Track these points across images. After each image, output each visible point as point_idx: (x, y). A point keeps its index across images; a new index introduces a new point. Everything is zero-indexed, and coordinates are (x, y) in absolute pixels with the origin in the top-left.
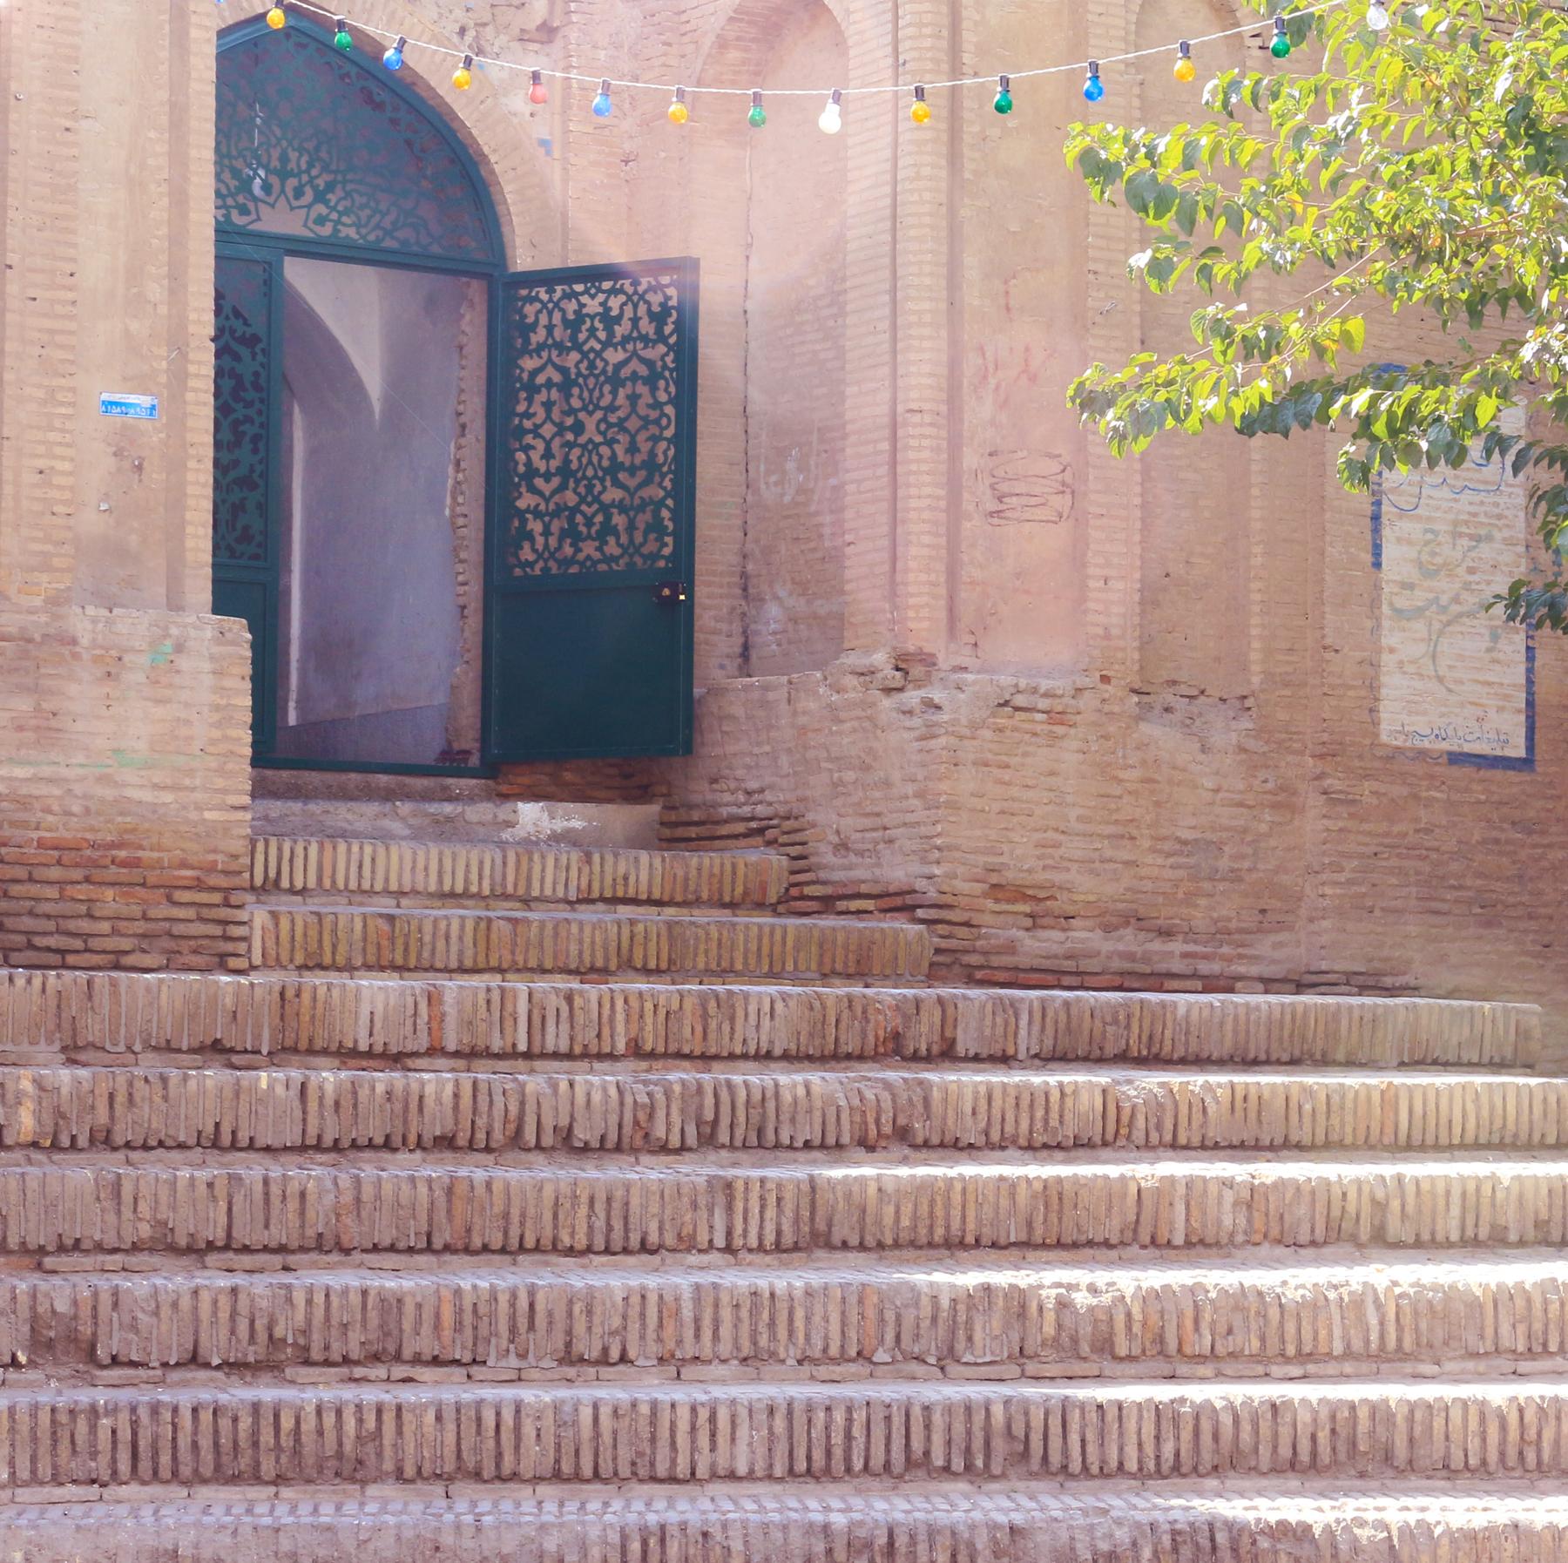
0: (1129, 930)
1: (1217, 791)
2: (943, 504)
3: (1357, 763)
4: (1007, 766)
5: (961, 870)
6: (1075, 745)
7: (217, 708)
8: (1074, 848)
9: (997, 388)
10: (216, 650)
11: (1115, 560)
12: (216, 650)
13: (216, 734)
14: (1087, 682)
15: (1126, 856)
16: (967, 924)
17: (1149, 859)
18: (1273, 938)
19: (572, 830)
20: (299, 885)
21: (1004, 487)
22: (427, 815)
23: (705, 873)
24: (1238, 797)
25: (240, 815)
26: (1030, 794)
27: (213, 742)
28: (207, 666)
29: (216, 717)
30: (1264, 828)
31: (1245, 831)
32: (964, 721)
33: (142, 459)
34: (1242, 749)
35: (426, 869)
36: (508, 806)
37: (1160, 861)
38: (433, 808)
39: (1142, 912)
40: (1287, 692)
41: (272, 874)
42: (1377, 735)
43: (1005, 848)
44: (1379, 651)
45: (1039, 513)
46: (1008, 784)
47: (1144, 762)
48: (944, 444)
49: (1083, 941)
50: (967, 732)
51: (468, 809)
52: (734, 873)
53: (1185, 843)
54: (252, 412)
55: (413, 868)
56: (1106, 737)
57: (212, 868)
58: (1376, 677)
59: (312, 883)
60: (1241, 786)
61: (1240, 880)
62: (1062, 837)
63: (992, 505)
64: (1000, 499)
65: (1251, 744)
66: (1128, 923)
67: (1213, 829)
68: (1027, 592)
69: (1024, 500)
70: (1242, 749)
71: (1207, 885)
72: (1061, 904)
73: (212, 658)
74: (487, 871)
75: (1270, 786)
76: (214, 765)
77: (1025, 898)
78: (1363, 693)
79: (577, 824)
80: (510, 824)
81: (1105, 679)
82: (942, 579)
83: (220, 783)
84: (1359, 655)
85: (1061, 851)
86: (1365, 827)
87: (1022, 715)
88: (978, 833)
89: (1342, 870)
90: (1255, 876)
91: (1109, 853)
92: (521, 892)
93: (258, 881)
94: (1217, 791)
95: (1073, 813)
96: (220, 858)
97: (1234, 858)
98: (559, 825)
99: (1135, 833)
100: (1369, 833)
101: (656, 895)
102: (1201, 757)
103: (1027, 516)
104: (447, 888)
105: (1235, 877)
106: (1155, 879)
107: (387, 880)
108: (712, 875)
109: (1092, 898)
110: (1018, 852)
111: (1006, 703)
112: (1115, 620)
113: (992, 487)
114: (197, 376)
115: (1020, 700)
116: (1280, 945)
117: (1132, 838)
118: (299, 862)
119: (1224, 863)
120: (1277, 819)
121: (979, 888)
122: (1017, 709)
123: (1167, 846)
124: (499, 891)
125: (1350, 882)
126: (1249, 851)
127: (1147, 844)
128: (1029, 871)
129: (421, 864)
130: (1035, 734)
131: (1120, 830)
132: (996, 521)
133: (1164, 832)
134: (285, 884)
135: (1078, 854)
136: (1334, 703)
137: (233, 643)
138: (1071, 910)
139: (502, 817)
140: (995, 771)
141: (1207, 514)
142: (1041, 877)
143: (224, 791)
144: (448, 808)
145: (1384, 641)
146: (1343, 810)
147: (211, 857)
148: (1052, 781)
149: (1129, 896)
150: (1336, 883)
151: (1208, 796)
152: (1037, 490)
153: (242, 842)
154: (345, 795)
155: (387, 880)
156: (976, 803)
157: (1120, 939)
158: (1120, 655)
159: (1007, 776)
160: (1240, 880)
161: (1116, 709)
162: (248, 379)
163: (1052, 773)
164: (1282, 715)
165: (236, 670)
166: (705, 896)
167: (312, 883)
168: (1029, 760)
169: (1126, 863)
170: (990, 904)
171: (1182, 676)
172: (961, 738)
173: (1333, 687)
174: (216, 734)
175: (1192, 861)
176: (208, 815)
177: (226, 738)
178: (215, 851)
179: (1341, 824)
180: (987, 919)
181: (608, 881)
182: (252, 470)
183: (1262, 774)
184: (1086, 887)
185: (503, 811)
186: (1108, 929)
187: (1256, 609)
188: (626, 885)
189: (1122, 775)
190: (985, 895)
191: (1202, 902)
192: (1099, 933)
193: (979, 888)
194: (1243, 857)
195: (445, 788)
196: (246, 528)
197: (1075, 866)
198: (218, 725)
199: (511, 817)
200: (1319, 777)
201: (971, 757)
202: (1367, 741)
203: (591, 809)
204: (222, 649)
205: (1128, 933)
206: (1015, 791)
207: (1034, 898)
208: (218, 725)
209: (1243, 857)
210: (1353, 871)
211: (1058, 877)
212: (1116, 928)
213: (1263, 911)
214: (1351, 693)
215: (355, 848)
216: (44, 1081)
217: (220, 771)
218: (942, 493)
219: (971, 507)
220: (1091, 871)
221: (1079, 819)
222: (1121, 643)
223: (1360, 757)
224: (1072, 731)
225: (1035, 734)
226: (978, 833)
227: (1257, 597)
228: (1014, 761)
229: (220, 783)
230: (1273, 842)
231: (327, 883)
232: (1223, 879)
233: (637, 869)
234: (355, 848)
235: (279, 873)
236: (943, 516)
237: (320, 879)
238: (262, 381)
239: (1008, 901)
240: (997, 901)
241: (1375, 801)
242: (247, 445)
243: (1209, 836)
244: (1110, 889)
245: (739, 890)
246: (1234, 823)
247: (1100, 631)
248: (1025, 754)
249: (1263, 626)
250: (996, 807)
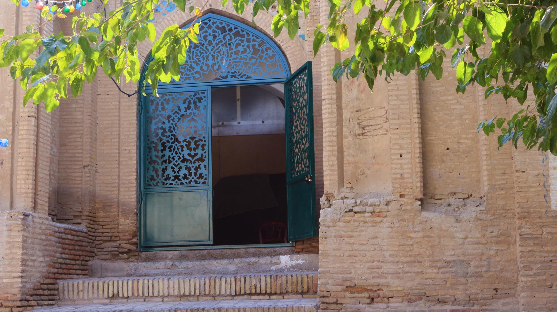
0: (422, 301)
1: (466, 238)
2: (335, 134)
3: (538, 220)
4: (352, 237)
5: (330, 281)
6: (387, 225)
7: (9, 243)
8: (388, 268)
9: (359, 85)
10: (8, 222)
11: (405, 146)
12: (8, 222)
13: (8, 252)
14: (392, 198)
15: (416, 270)
16: (336, 303)
17: (430, 271)
18: (502, 301)
19: (298, 264)
20: (126, 296)
21: (365, 123)
22: (246, 262)
23: (290, 282)
24: (477, 240)
25: (16, 280)
26: (364, 247)
27: (7, 255)
28: (5, 229)
29: (8, 246)
30: (492, 252)
31: (482, 254)
32: (329, 220)
33: (3, 160)
34: (478, 219)
35: (173, 287)
36: (277, 257)
37: (435, 271)
38: (247, 260)
39: (428, 293)
40: (503, 192)
41: (116, 292)
42: (550, 207)
43: (353, 271)
44: (548, 170)
45: (381, 132)
46: (353, 244)
47: (424, 230)
48: (335, 110)
49: (396, 307)
50: (331, 224)
51: (261, 260)
52: (302, 281)
53: (449, 262)
54: (169, 139)
55: (168, 287)
56: (403, 220)
57: (6, 299)
58: (547, 181)
59: (130, 295)
60: (478, 235)
61: (482, 276)
62: (382, 264)
63: (360, 131)
64: (363, 128)
65: (483, 217)
66: (421, 299)
67: (464, 255)
68: (378, 164)
69: (374, 127)
70: (478, 219)
71: (463, 280)
72: (386, 292)
73: (7, 225)
74: (197, 287)
75: (494, 234)
76: (7, 263)
77: (367, 290)
78: (539, 189)
79: (300, 262)
80: (278, 264)
81: (401, 196)
82: (335, 163)
83: (9, 269)
84: (536, 172)
85: (381, 270)
86: (545, 249)
87: (359, 215)
88: (338, 265)
89: (532, 269)
90: (489, 274)
91: (407, 269)
92: (212, 293)
93: (111, 295)
94: (466, 238)
95: (387, 254)
96: (9, 295)
97: (477, 267)
98: (294, 263)
99: (421, 259)
100: (547, 251)
101: (269, 291)
102: (456, 224)
103: (375, 133)
104: (182, 293)
105: (478, 275)
106: (433, 279)
107: (159, 292)
108: (292, 283)
109: (399, 289)
110: (359, 272)
111: (351, 211)
112: (406, 171)
113: (359, 124)
114: (22, 130)
115: (356, 209)
116: (508, 304)
117: (419, 262)
118: (125, 287)
119: (471, 270)
120: (500, 248)
121: (339, 288)
122: (356, 213)
123: (439, 264)
124: (203, 293)
125: (535, 274)
126: (485, 263)
127: (427, 264)
128: (366, 279)
129: (171, 286)
130: (365, 222)
131: (413, 259)
132: (362, 137)
133: (437, 258)
134: (121, 295)
135: (391, 271)
136: (523, 195)
137: (15, 220)
138: (390, 295)
139: (274, 261)
140: (347, 240)
141: (467, 121)
142: (372, 281)
143: (11, 272)
144: (253, 260)
145: (550, 165)
146: (531, 242)
147: (6, 295)
148: (375, 241)
149: (419, 287)
150: (528, 276)
151: (461, 241)
152: (378, 123)
153: (18, 289)
154: (216, 258)
155: (159, 292)
156: (337, 253)
157: (417, 305)
158: (409, 185)
159: (351, 240)
160: (482, 276)
161: (409, 208)
162: (167, 129)
163: (376, 238)
164: (501, 202)
165: (16, 229)
166: (290, 290)
167: (130, 295)
168: (363, 233)
169: (417, 273)
170: (348, 294)
171: (459, 190)
172: (329, 227)
173: (521, 188)
174: (8, 252)
175: (453, 269)
176: (4, 281)
177: (12, 253)
178: (7, 293)
179: (530, 248)
180: (347, 301)
181: (248, 287)
182: (169, 157)
183: (490, 229)
184: (395, 284)
185: (275, 260)
186: (410, 301)
187: (484, 158)
188: (256, 288)
189: (412, 235)
190: (344, 291)
191: (461, 287)
192: (405, 303)
193: (339, 288)
194: (482, 266)
195: (275, 251)
196: (201, 174)
197: (390, 276)
198: (9, 249)
199: (278, 261)
200: (519, 228)
201: (333, 234)
202: (544, 210)
203: (306, 256)
204: (11, 222)
205: (421, 303)
206: (356, 247)
207: (371, 290)
208: (9, 249)
209: (482, 266)
210: (538, 269)
211: (381, 281)
212: (415, 301)
213: (496, 290)
214: (532, 189)
215: (146, 282)
216: (556, 299)
217: (9, 265)
218: (335, 129)
219: (347, 134)
220: (398, 277)
221: (390, 256)
222: (411, 180)
223: (540, 217)
224: (385, 219)
225: (365, 222)
226: (338, 265)
227: (484, 153)
228: (355, 234)
229: (9, 269)
230: (498, 259)
231: (136, 294)
232: (471, 277)
233: (260, 282)
234: (146, 282)
235: (118, 292)
236: (335, 139)
237: (133, 293)
238: (172, 129)
239: (359, 292)
240: (352, 292)
241: (550, 237)
242: (167, 149)
243: (462, 258)
244: (409, 284)
245: (305, 287)
246: (475, 252)
247: (399, 176)
248: (361, 231)
249: (488, 165)
250: (347, 254)
